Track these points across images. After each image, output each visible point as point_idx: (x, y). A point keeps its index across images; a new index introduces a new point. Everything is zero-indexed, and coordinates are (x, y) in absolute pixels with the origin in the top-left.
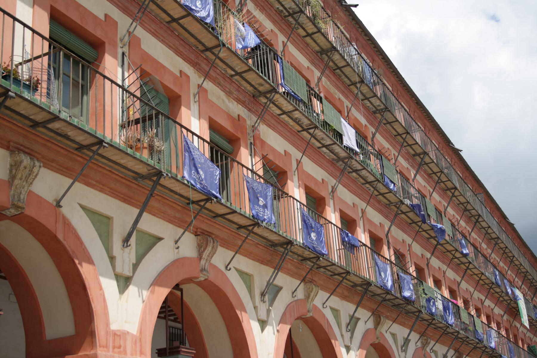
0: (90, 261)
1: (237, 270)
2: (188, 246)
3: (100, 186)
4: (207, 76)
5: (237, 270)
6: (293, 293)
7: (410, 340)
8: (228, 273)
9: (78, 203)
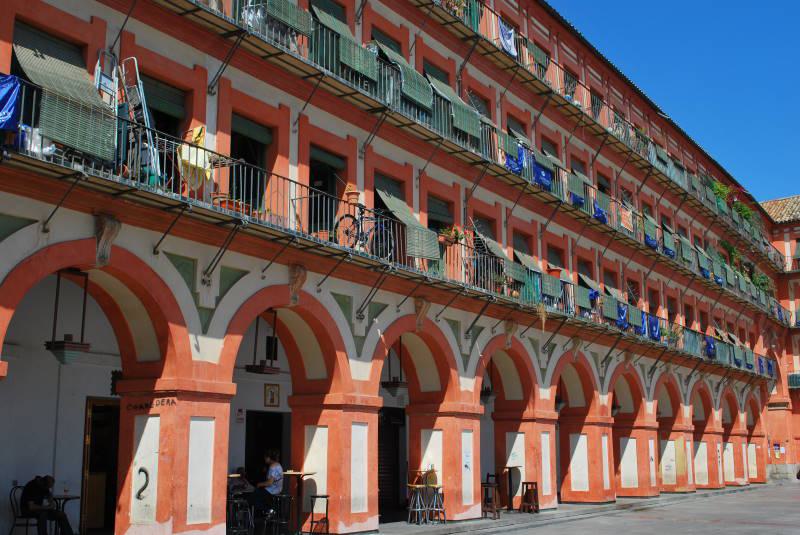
0: (456, 369)
1: (165, 253)
2: (500, 329)
3: (343, 276)
4: (694, 218)
5: (165, 253)
6: (155, 248)
7: (611, 358)
8: (439, 324)
9: (332, 294)
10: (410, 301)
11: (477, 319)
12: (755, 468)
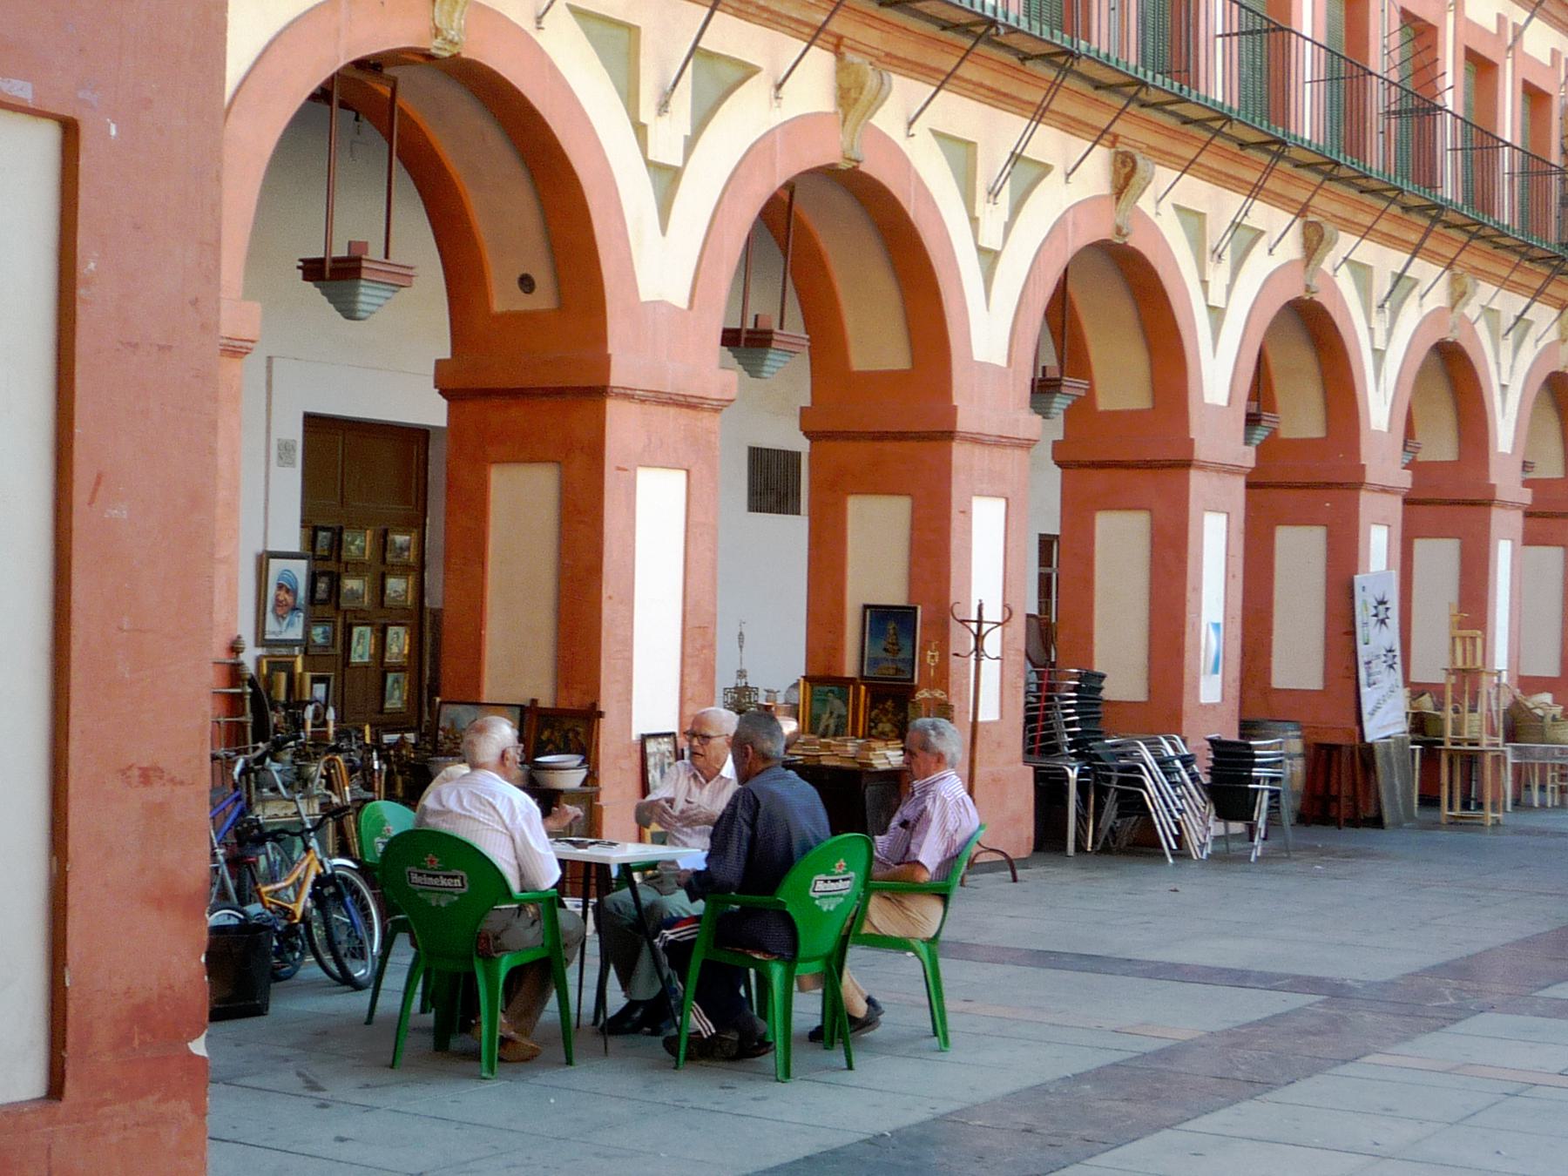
7: (1530, 323)
10: (820, 61)
11: (1528, 307)
12: (441, 542)
